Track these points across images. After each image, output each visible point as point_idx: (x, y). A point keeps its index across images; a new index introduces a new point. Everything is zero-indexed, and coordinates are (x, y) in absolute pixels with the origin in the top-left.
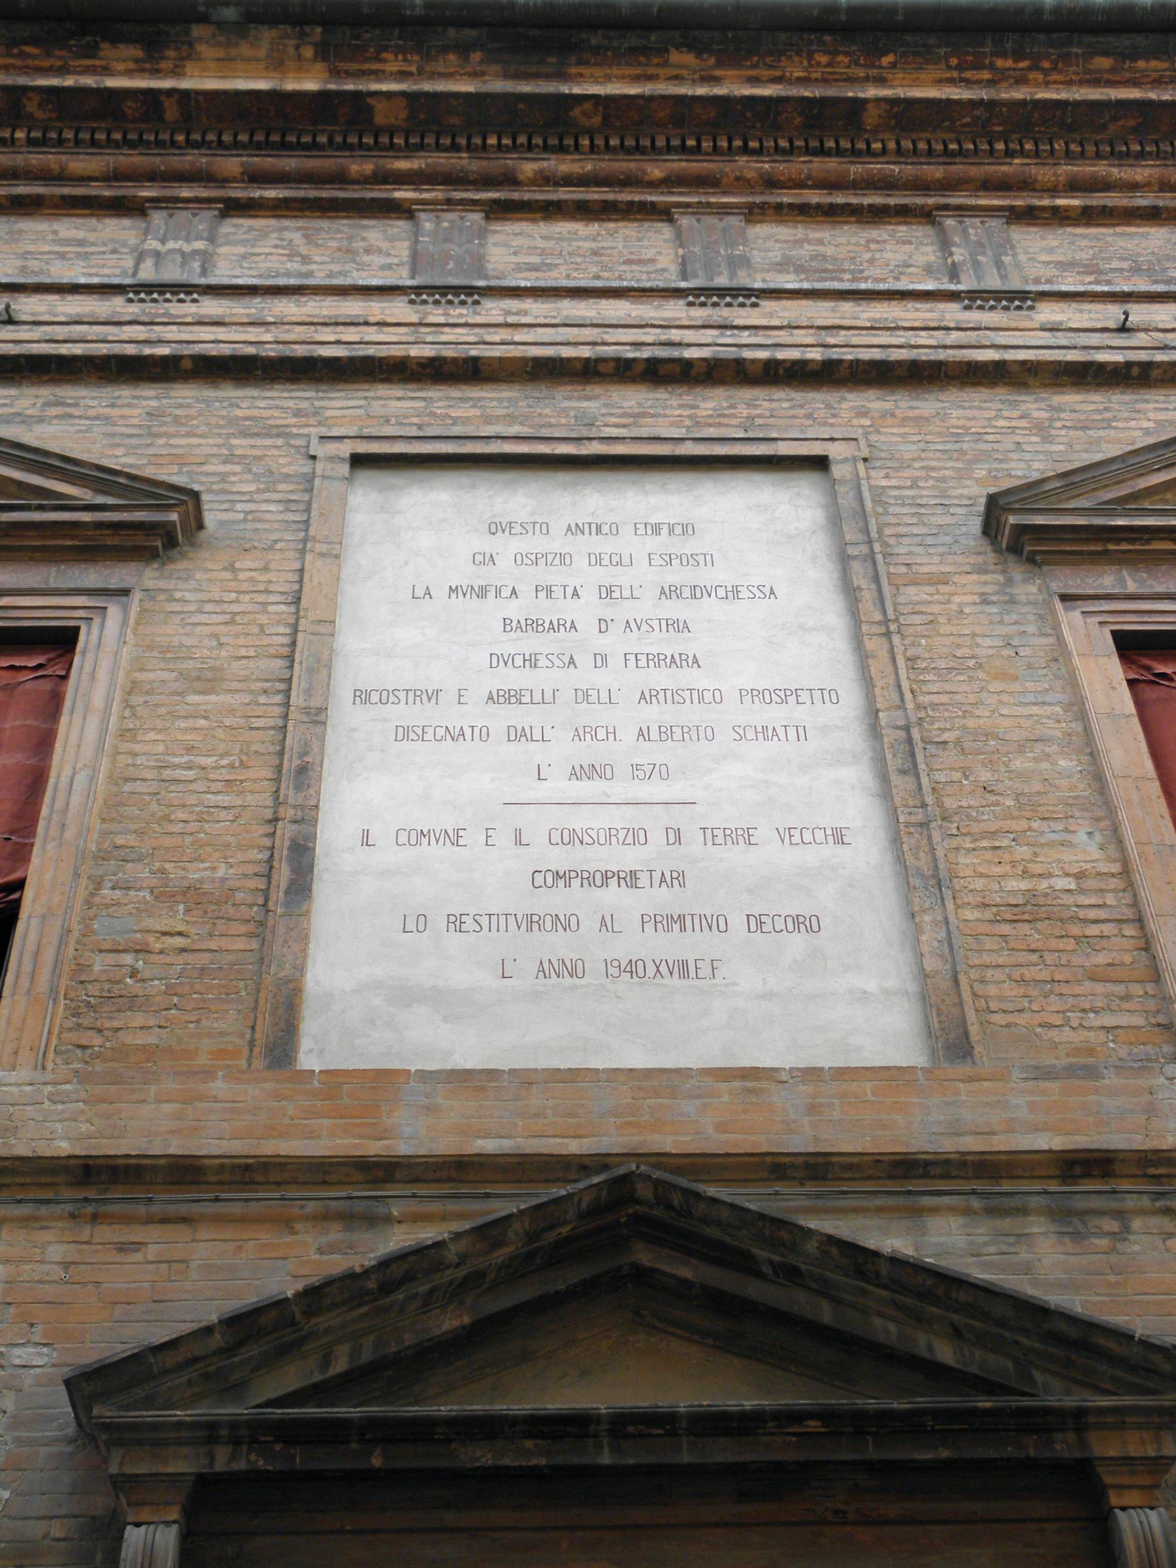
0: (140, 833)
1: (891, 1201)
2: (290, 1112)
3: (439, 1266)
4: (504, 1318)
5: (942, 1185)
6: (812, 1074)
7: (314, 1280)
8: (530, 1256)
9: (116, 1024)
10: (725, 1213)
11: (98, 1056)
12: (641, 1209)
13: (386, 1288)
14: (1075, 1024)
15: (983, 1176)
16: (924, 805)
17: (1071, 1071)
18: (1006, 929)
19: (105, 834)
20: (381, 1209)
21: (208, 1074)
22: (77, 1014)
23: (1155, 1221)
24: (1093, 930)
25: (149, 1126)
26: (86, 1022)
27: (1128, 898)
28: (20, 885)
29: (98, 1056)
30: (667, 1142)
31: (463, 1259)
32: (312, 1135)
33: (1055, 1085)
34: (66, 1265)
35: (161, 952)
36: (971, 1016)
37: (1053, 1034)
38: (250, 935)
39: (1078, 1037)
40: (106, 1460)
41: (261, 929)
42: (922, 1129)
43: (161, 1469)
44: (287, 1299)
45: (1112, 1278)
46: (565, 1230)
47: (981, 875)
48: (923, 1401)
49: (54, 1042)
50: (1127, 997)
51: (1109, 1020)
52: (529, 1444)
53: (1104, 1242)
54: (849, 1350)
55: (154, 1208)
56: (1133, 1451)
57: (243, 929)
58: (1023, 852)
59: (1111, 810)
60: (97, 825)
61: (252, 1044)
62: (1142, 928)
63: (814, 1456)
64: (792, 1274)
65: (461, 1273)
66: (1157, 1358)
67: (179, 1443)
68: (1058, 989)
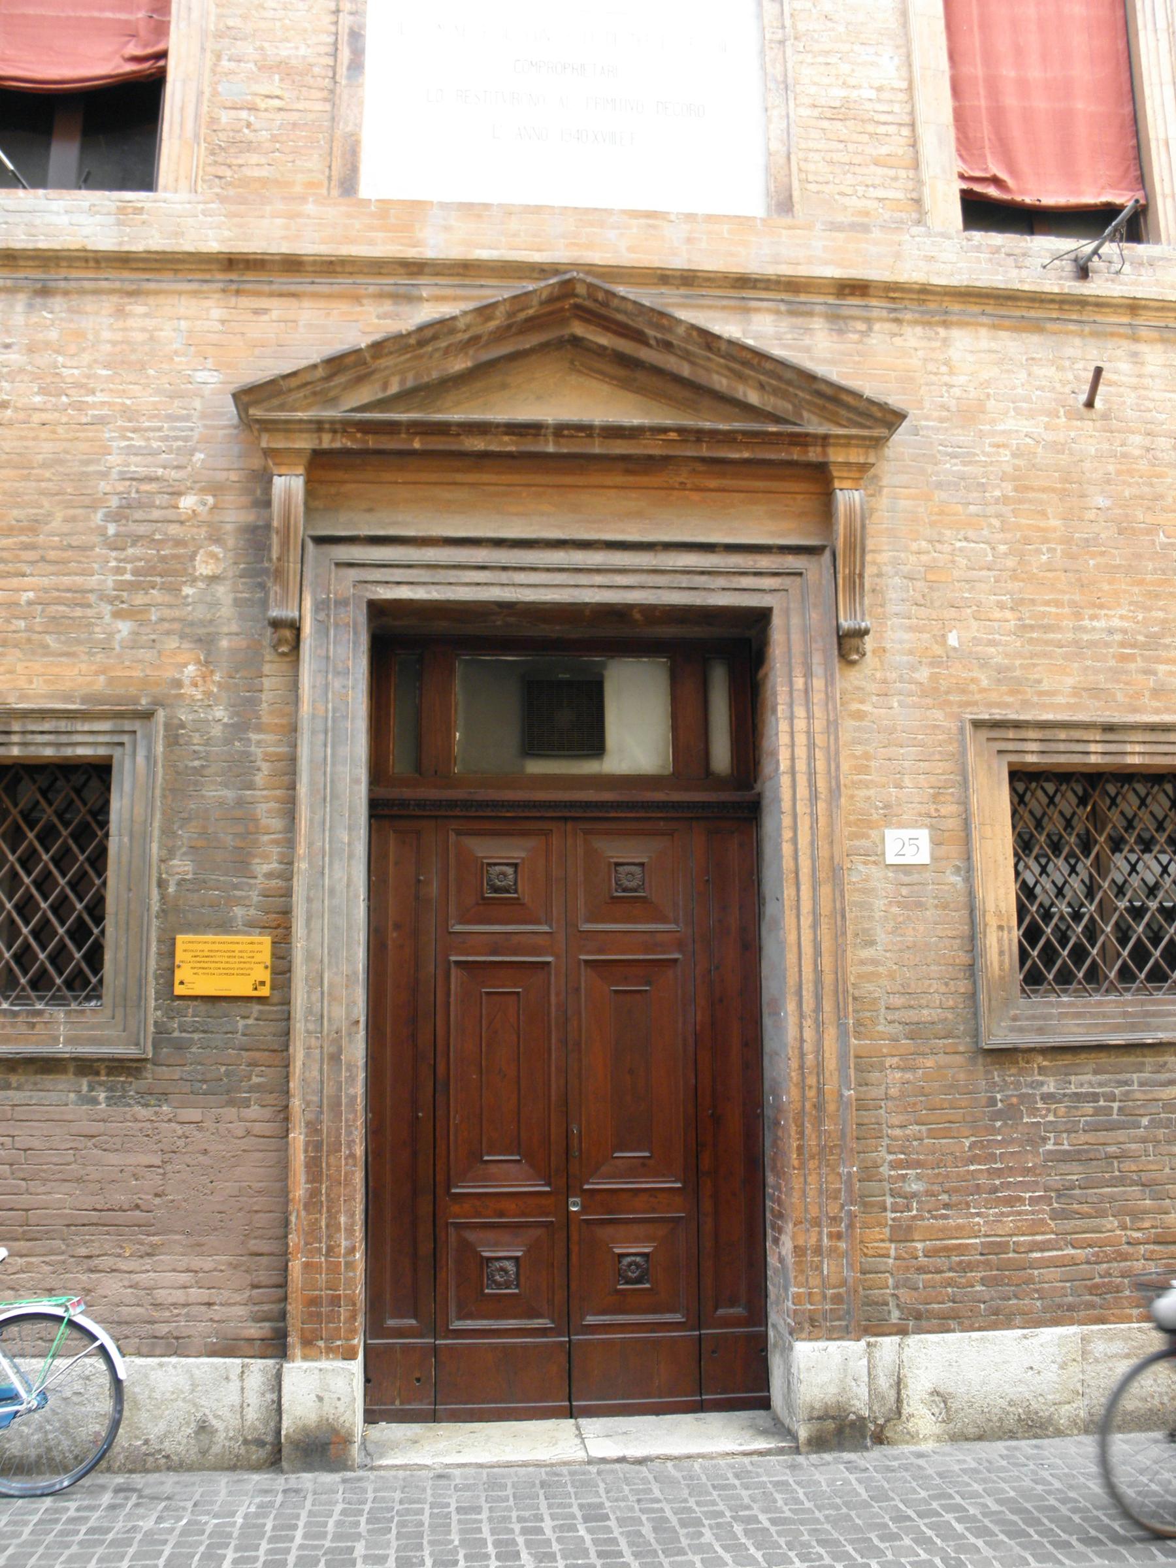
0: (245, 17)
1: (732, 303)
2: (357, 226)
3: (453, 331)
4: (492, 364)
5: (764, 295)
6: (690, 217)
7: (377, 337)
8: (509, 327)
9: (240, 161)
10: (630, 307)
11: (230, 184)
12: (579, 301)
13: (421, 344)
14: (860, 194)
15: (790, 290)
16: (783, 27)
17: (853, 227)
18: (825, 124)
19: (220, 16)
20: (415, 292)
21: (303, 199)
22: (213, 154)
23: (888, 326)
24: (882, 129)
25: (266, 235)
26: (220, 159)
27: (908, 108)
28: (163, 55)
29: (230, 184)
30: (598, 257)
31: (468, 327)
32: (371, 243)
33: (841, 236)
34: (223, 322)
35: (266, 110)
36: (796, 185)
37: (846, 201)
38: (325, 100)
39: (860, 204)
40: (259, 438)
41: (331, 96)
42: (757, 257)
43: (291, 445)
44: (360, 350)
45: (857, 359)
46: (531, 312)
47: (815, 84)
48: (737, 426)
49: (201, 173)
50: (896, 179)
51: (881, 193)
52: (506, 438)
53: (855, 337)
54: (697, 392)
55: (274, 287)
56: (853, 459)
57: (320, 95)
58: (845, 68)
59: (908, 42)
60: (213, 9)
61: (330, 178)
62: (913, 130)
63: (671, 453)
64: (668, 346)
65: (466, 336)
66: (874, 409)
67: (301, 431)
68: (852, 169)
